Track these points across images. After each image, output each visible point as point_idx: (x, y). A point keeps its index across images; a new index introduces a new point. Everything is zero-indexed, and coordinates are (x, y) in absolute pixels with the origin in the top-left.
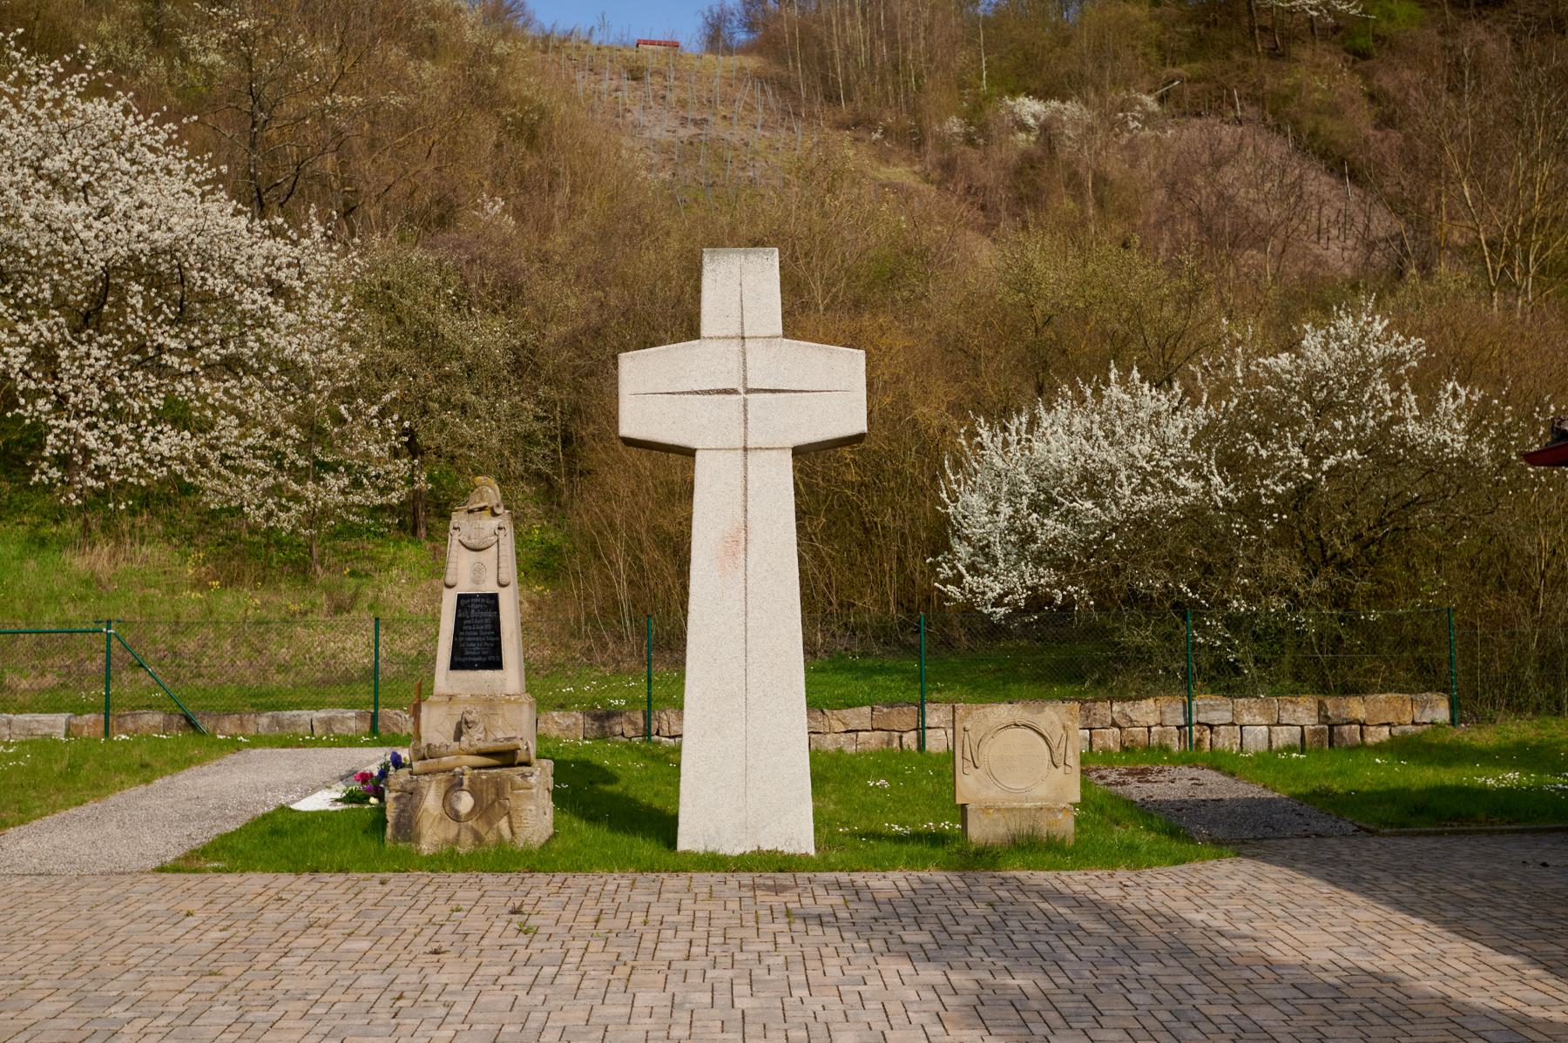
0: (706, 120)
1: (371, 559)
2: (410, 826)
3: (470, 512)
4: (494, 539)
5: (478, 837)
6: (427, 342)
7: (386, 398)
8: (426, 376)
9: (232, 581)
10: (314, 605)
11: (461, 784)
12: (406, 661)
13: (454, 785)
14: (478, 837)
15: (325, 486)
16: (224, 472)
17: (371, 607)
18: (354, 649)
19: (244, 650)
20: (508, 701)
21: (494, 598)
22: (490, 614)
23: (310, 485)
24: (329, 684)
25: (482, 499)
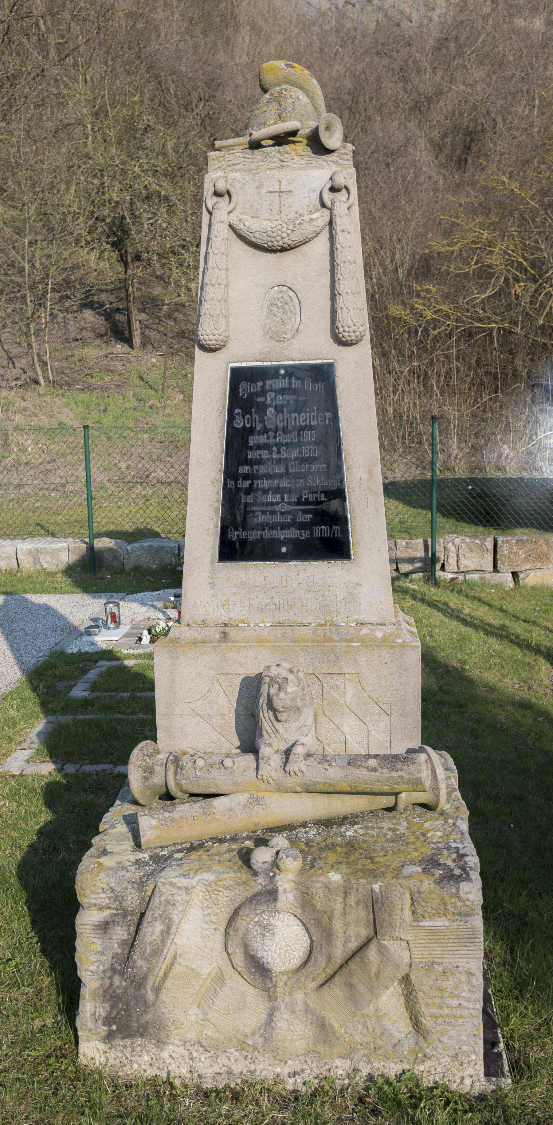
11: (271, 895)
21: (322, 375)
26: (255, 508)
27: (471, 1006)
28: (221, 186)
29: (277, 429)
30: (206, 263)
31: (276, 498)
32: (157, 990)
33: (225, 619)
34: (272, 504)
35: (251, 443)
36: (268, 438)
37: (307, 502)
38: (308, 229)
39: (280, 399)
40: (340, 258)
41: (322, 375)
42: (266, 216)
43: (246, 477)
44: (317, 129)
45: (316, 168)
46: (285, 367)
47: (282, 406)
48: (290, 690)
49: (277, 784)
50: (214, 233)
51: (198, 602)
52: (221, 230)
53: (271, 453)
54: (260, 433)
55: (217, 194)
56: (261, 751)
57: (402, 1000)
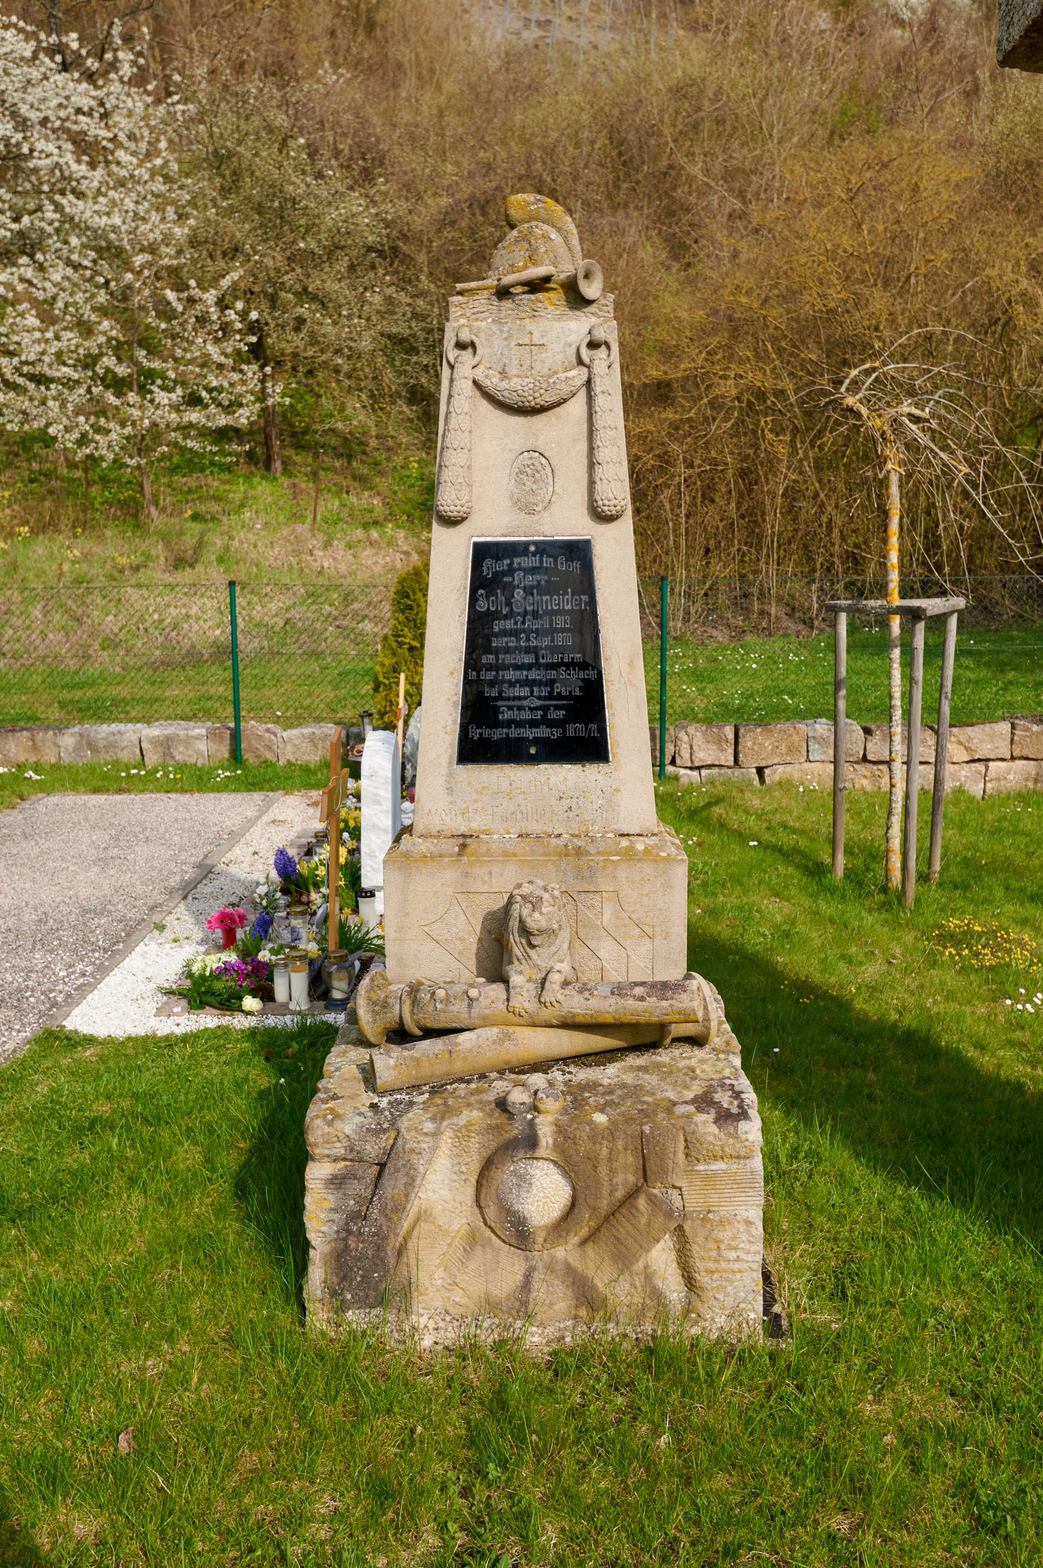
0: (549, 22)
1: (217, 499)
2: (378, 1261)
3: (503, 293)
4: (579, 375)
5: (587, 1298)
6: (277, 215)
7: (225, 283)
8: (274, 259)
9: (45, 527)
10: (148, 557)
11: (531, 1141)
12: (270, 632)
13: (511, 1143)
14: (587, 1298)
15: (152, 401)
16: (20, 381)
17: (221, 560)
18: (203, 619)
19: (58, 618)
20: (629, 855)
21: (579, 552)
22: (568, 602)
23: (132, 397)
24: (164, 676)
25: (532, 260)
26: (500, 703)
27: (750, 1258)
28: (465, 336)
29: (525, 613)
30: (446, 424)
31: (525, 692)
32: (400, 1252)
33: (463, 830)
34: (519, 698)
35: (496, 629)
36: (516, 623)
37: (560, 696)
38: (564, 390)
39: (530, 580)
40: (599, 422)
41: (579, 552)
42: (515, 372)
43: (490, 667)
44: (575, 277)
45: (571, 319)
46: (536, 543)
47: (532, 587)
48: (544, 910)
49: (531, 1016)
50: (456, 389)
51: (433, 810)
52: (464, 387)
53: (519, 640)
54: (506, 617)
55: (461, 346)
56: (511, 980)
57: (673, 1255)
